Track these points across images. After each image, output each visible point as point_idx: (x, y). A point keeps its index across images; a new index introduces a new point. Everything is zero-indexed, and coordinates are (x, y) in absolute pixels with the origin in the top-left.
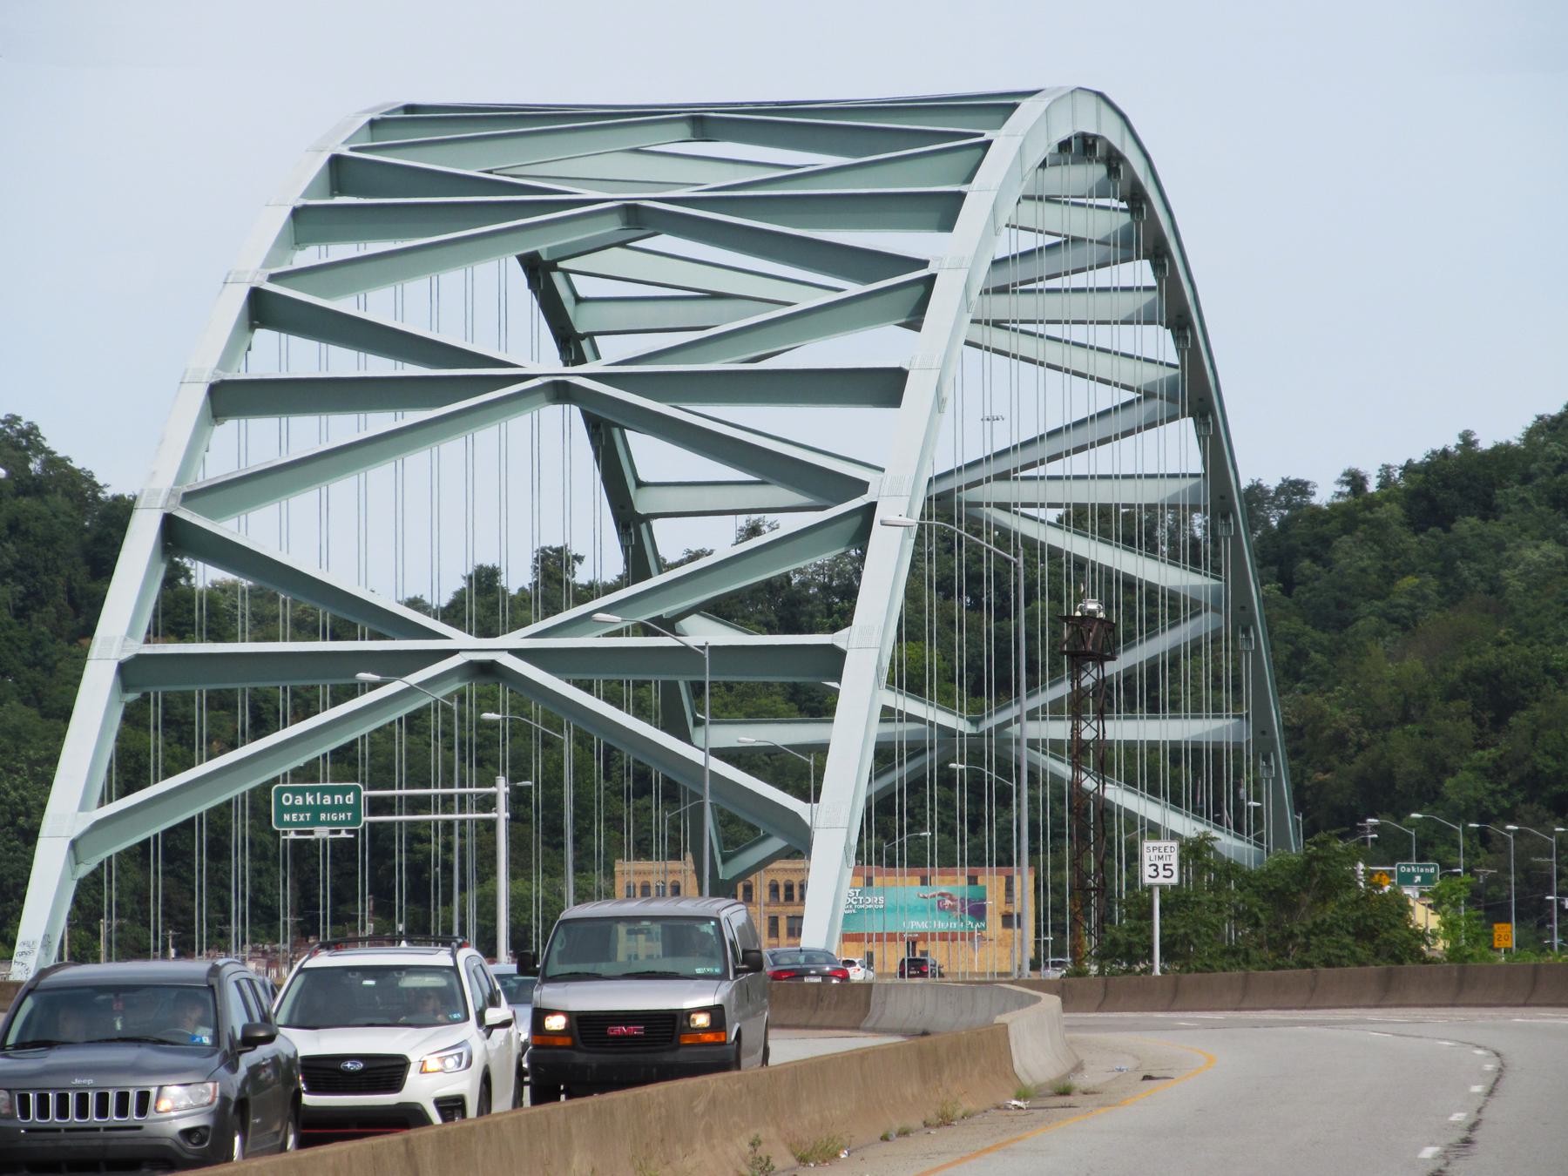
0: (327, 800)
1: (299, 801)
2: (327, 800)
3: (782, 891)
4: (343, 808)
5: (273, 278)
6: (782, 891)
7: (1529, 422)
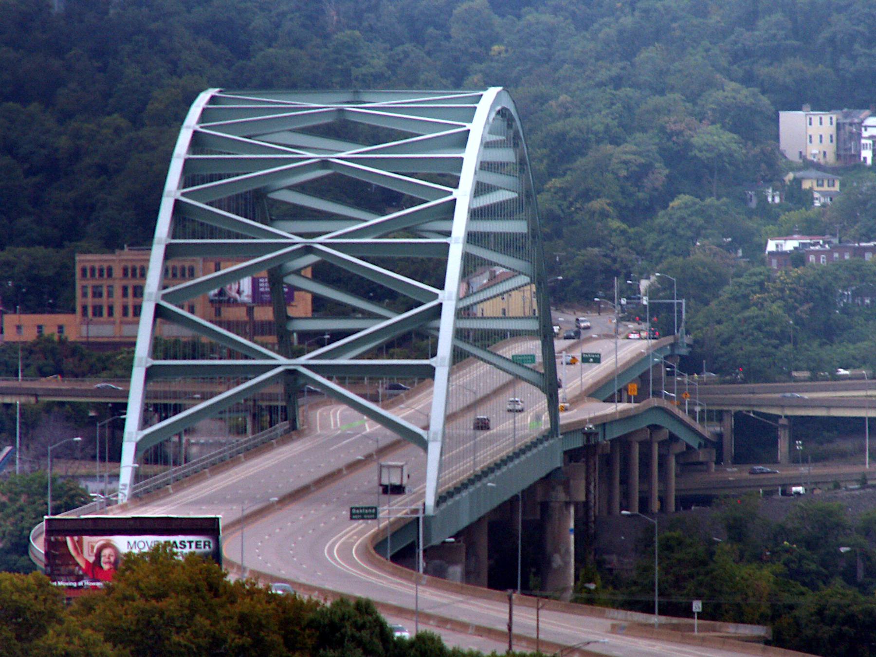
0: (366, 511)
1: (358, 511)
2: (366, 511)
3: (130, 271)
4: (371, 514)
6: (130, 271)
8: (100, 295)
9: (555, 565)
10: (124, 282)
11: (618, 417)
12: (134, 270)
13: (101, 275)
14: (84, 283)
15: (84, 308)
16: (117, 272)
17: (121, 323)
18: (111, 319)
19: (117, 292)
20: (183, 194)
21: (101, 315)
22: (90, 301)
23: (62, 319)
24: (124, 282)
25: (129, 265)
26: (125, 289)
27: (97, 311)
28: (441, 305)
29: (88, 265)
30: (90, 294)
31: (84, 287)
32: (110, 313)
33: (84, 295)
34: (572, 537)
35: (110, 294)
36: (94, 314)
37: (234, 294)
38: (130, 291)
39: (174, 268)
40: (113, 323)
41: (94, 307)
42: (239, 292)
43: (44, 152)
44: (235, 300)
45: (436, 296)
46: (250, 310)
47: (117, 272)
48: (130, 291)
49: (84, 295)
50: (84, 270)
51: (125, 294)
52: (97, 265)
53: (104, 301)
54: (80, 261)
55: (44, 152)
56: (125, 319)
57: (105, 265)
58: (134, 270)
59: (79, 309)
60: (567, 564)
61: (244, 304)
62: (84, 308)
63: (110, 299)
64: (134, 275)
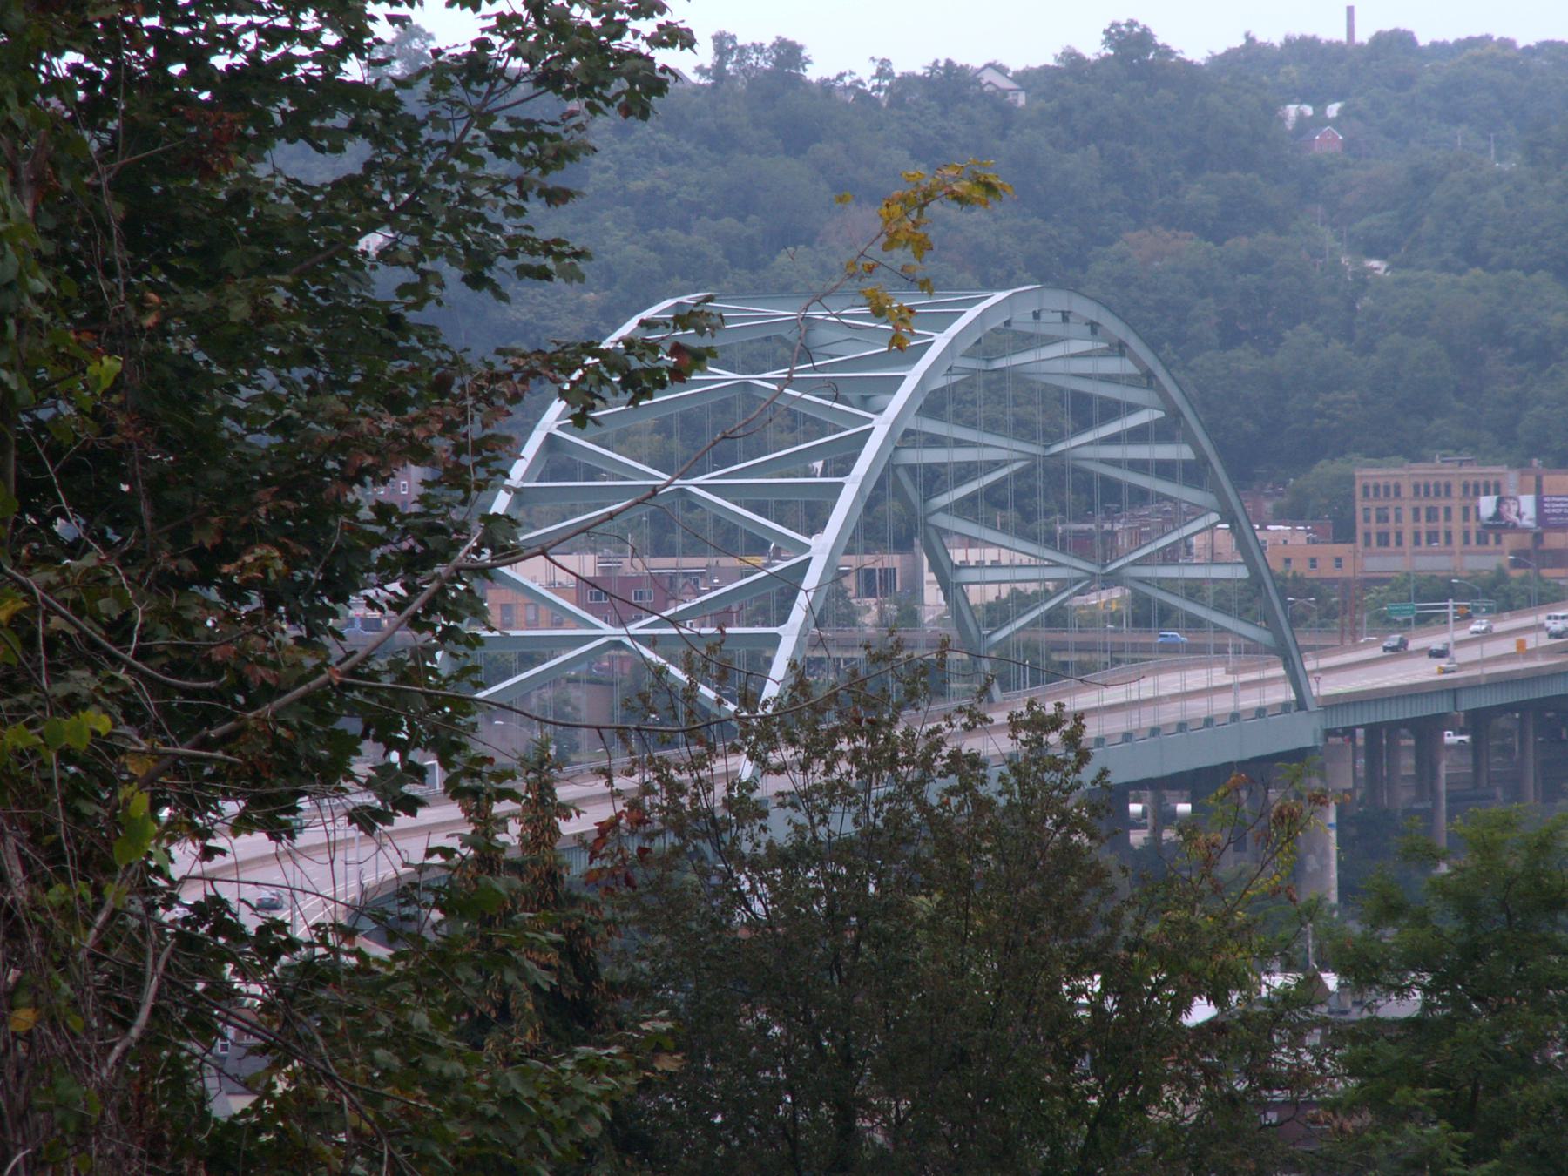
3: (1443, 489)
7: (1476, 33)
8: (1387, 520)
9: (1309, 869)
10: (1416, 503)
11: (1483, 681)
12: (1427, 487)
13: (1387, 494)
14: (1367, 504)
15: (1367, 535)
16: (1407, 491)
17: (1462, 553)
19: (1408, 515)
20: (870, 420)
21: (1387, 544)
22: (1374, 527)
23: (1341, 549)
24: (1416, 503)
25: (1432, 481)
26: (1416, 511)
27: (1383, 539)
28: (810, 559)
29: (1371, 482)
30: (1373, 519)
31: (1366, 509)
32: (1399, 543)
33: (1367, 519)
34: (1333, 834)
35: (1398, 518)
36: (1379, 544)
37: (1513, 517)
38: (1423, 513)
39: (1437, 485)
40: (1404, 554)
41: (1379, 535)
42: (1519, 515)
43: (1535, 331)
44: (1515, 525)
45: (807, 548)
46: (1538, 538)
47: (1407, 491)
48: (1423, 513)
49: (1367, 519)
50: (1366, 488)
51: (1417, 518)
52: (1381, 482)
53: (1391, 526)
54: (1362, 477)
55: (1535, 331)
56: (1467, 548)
58: (1427, 487)
59: (1360, 537)
60: (1325, 867)
61: (1525, 530)
62: (1367, 535)
64: (1427, 494)
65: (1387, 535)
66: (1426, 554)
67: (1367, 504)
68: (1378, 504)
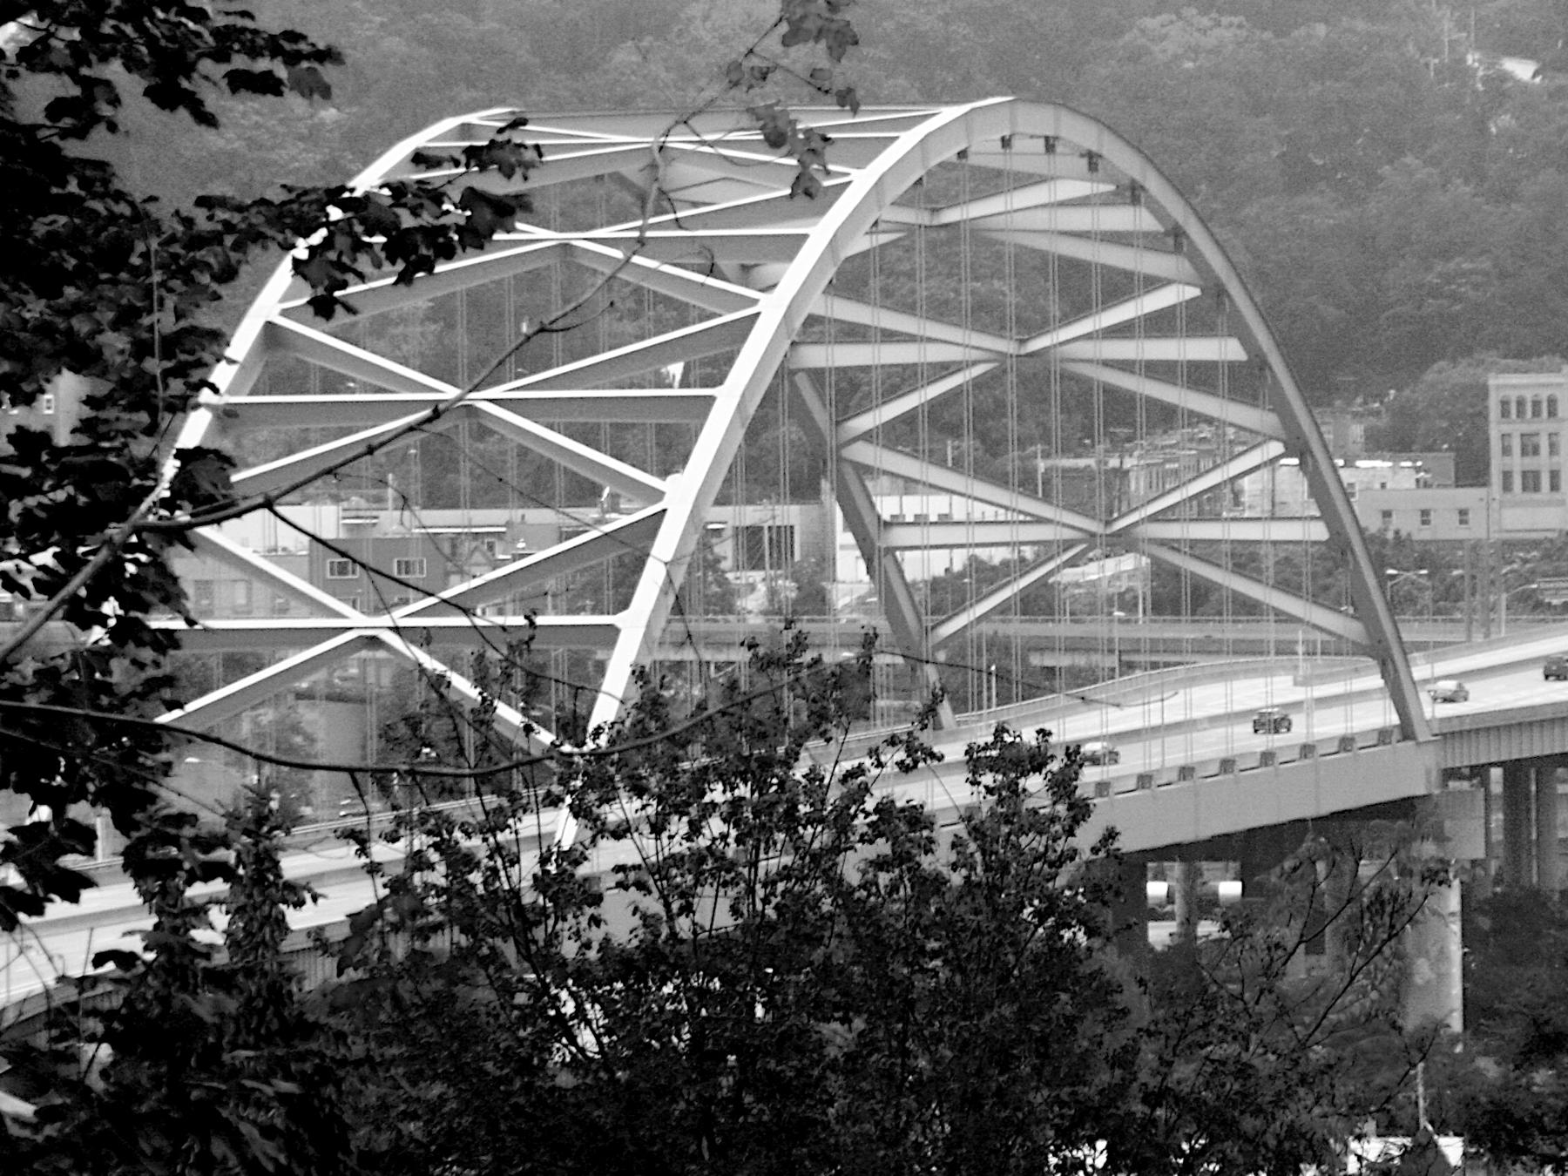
5: (847, 174)
14: (1506, 428)
15: (1507, 476)
18: (1557, 496)
21: (1537, 488)
22: (1517, 463)
33: (1506, 451)
39: (1521, 403)
54: (1498, 387)
56: (1508, 496)
57: (1544, 395)
62: (1507, 476)
63: (1555, 459)
65: (1536, 475)
66: (1549, 503)
67: (1506, 428)
68: (1525, 428)
